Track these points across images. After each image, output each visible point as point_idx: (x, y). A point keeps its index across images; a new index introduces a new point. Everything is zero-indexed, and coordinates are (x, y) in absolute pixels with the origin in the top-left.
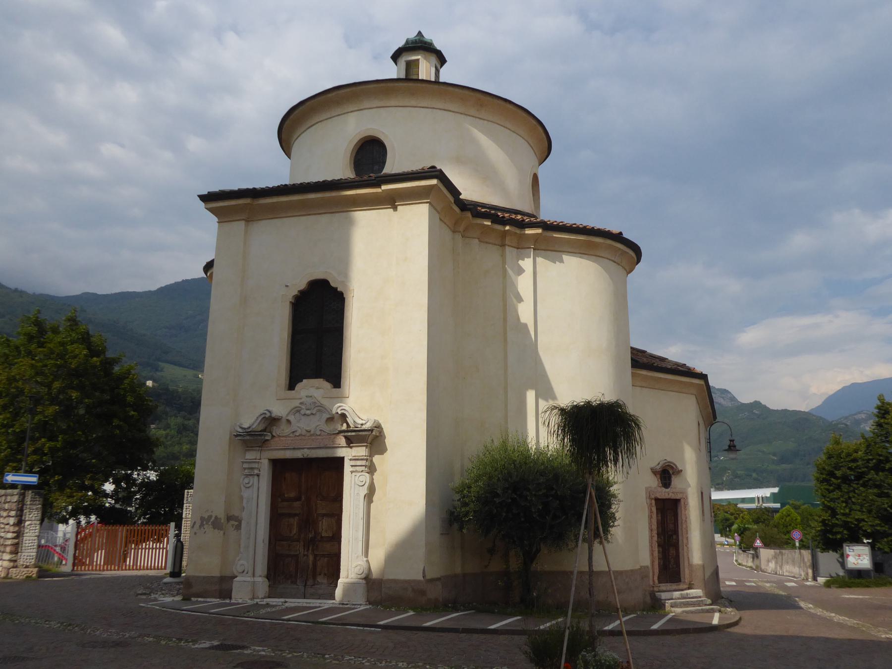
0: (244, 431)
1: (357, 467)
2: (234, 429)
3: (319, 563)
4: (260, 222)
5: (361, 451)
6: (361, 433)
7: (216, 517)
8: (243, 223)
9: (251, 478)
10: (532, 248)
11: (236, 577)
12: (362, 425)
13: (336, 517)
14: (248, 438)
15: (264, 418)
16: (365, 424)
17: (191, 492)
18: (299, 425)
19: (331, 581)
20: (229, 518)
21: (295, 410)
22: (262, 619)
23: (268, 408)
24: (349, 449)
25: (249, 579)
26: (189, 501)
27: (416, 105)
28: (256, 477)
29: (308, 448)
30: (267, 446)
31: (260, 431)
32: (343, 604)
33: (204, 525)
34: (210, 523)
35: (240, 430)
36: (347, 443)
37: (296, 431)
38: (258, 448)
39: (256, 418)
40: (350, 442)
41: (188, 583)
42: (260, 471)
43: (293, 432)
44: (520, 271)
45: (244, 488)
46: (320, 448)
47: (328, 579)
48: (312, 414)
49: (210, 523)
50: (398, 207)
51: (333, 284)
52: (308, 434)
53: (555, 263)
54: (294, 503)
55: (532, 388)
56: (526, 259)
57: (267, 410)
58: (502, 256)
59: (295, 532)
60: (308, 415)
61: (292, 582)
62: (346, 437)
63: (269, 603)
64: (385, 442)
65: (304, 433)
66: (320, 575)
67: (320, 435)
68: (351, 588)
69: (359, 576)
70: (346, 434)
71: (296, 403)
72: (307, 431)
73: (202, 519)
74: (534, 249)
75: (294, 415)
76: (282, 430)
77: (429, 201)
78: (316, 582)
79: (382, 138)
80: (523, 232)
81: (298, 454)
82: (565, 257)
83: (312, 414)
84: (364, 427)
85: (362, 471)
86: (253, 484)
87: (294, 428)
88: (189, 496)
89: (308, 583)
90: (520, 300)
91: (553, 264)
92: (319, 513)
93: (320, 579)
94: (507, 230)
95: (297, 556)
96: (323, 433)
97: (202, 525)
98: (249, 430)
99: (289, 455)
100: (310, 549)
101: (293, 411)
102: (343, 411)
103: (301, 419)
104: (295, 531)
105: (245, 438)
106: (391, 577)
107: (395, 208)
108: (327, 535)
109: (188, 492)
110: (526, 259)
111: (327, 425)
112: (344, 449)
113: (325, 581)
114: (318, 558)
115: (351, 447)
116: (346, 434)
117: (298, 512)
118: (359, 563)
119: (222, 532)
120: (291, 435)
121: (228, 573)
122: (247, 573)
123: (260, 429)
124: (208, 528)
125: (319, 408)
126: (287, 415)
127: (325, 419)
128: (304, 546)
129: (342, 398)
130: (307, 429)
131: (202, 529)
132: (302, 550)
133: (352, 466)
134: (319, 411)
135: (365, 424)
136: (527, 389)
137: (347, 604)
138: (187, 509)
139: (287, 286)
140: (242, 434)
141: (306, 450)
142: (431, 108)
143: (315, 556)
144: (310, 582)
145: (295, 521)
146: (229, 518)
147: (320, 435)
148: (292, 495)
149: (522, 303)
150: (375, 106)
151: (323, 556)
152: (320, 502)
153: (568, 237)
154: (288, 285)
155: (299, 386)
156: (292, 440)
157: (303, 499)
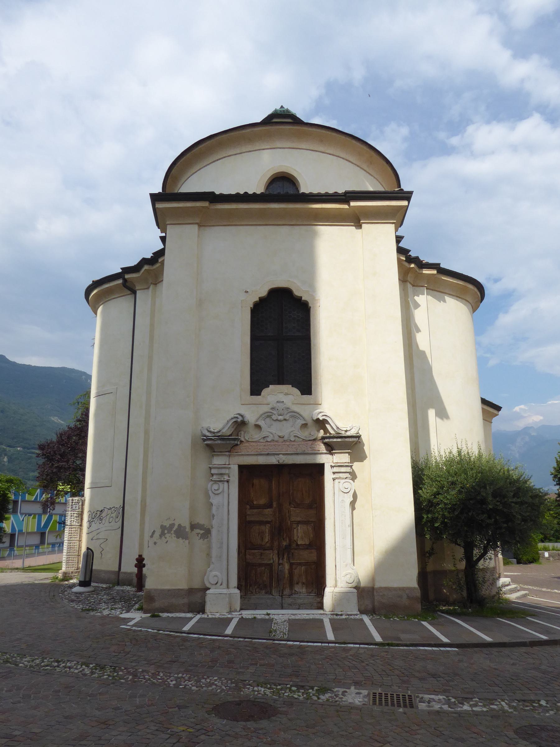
0: (213, 435)
1: (341, 474)
2: (202, 432)
3: (296, 572)
4: (213, 227)
5: (343, 458)
6: (347, 440)
7: (180, 526)
8: (196, 227)
9: (220, 484)
10: (426, 286)
11: (209, 589)
12: (346, 431)
13: (312, 524)
14: (219, 442)
15: (235, 421)
16: (350, 430)
17: (75, 500)
18: (269, 430)
19: (310, 590)
20: (193, 527)
21: (266, 415)
22: (308, 642)
23: (239, 412)
24: (329, 456)
25: (225, 591)
26: (74, 508)
27: (323, 151)
28: (226, 484)
29: (283, 454)
30: (236, 451)
31: (229, 436)
32: (337, 615)
33: (165, 534)
34: (172, 532)
35: (208, 434)
36: (327, 450)
37: (268, 437)
38: (228, 453)
39: (226, 421)
40: (331, 449)
41: (150, 597)
42: (229, 477)
43: (264, 438)
44: (417, 306)
45: (213, 495)
46: (297, 454)
47: (306, 588)
48: (285, 420)
49: (172, 532)
50: (363, 225)
51: (297, 293)
52: (281, 440)
53: (440, 302)
54: (265, 510)
55: (433, 408)
56: (420, 295)
57: (239, 414)
58: (404, 290)
59: (267, 540)
60: (280, 421)
61: (266, 593)
62: (325, 444)
63: (256, 616)
64: (364, 449)
65: (276, 438)
66: (297, 583)
67: (294, 441)
68: (342, 598)
69: (350, 585)
70: (327, 440)
71: (266, 409)
72: (280, 437)
73: (163, 528)
74: (427, 289)
75: (264, 420)
76: (250, 435)
77: (395, 221)
78: (293, 592)
79: (295, 175)
80: (421, 272)
81: (273, 460)
82: (447, 298)
83: (285, 420)
84: (348, 434)
85: (346, 478)
86: (223, 491)
87: (264, 434)
88: (74, 503)
89: (285, 593)
90: (418, 330)
91: (439, 302)
92: (293, 520)
93: (297, 588)
94: (412, 268)
95: (271, 565)
96: (297, 439)
97: (162, 534)
98: (219, 435)
99: (262, 460)
100: (285, 557)
101: (263, 416)
102: (324, 417)
103: (272, 425)
104: (267, 538)
105: (216, 442)
106: (383, 585)
107: (359, 226)
108: (304, 543)
109: (73, 500)
110: (420, 295)
111: (301, 430)
112: (324, 456)
113: (304, 590)
114: (294, 567)
115: (332, 454)
116: (327, 440)
117: (269, 520)
118: (350, 572)
119: (187, 541)
120: (262, 441)
121: (196, 584)
122: (221, 585)
123: (229, 434)
124: (171, 538)
125: (294, 414)
126: (257, 420)
127: (300, 425)
128: (278, 553)
129: (317, 404)
130: (280, 434)
131: (163, 538)
132: (276, 558)
133: (334, 473)
134: (292, 416)
135: (350, 430)
136: (429, 408)
137: (341, 615)
138: (71, 516)
139: (247, 292)
140: (213, 438)
141: (281, 456)
142: (336, 156)
143: (291, 565)
144: (287, 591)
145: (266, 529)
146: (193, 527)
147: (294, 441)
148: (262, 501)
149: (420, 333)
150: (287, 147)
151: (300, 564)
152: (294, 509)
153: (452, 281)
154: (248, 291)
155: (265, 392)
156: (264, 446)
157: (275, 505)
